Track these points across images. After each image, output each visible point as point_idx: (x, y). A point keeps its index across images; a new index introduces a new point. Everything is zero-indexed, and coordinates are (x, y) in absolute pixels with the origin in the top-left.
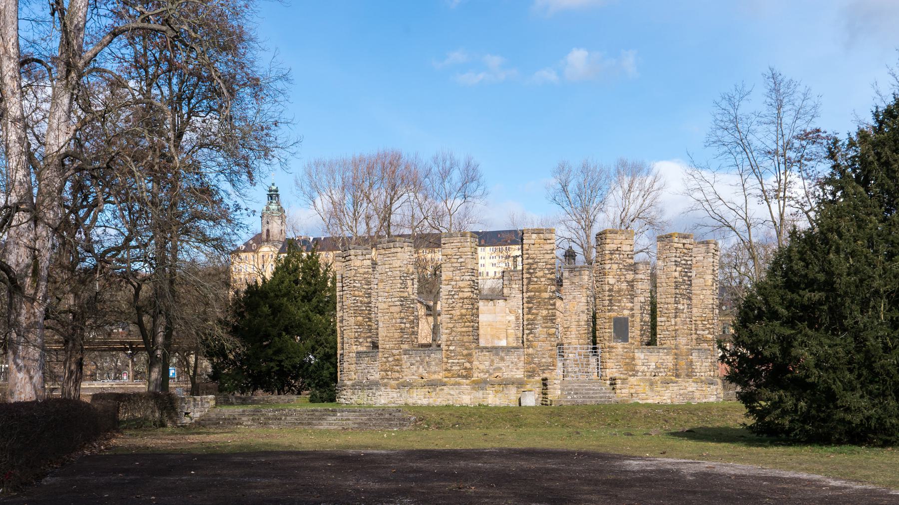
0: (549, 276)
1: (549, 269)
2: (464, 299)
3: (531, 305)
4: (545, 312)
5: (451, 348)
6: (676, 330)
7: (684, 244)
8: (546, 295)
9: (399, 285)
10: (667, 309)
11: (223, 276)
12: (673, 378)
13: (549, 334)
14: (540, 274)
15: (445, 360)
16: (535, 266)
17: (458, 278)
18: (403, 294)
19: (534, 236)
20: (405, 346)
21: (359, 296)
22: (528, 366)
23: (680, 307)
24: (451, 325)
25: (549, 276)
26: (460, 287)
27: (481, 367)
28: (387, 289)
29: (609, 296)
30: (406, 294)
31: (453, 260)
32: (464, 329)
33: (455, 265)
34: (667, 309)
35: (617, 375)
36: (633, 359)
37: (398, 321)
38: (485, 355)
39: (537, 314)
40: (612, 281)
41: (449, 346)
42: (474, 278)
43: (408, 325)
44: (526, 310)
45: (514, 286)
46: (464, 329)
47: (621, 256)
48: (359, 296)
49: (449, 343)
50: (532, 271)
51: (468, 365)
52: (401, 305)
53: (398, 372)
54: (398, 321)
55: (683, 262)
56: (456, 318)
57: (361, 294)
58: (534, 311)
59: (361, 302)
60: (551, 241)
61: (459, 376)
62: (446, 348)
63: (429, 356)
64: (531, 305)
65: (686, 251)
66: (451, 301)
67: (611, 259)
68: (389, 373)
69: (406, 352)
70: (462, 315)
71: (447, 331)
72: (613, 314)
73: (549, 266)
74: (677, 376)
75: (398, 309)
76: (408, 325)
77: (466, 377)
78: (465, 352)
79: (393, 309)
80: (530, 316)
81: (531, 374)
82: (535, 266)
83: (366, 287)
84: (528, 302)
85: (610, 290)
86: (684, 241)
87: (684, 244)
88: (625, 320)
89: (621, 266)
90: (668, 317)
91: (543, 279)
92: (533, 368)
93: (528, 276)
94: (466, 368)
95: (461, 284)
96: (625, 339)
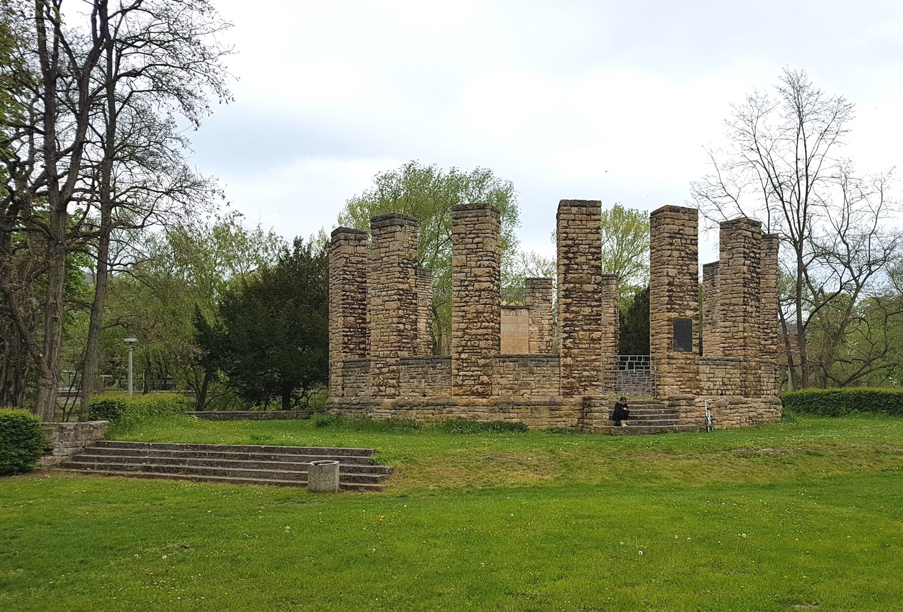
0: (593, 262)
1: (593, 254)
2: (480, 290)
3: (569, 301)
4: (587, 310)
5: (463, 356)
6: (745, 338)
7: (753, 232)
8: (589, 288)
9: (398, 275)
10: (733, 311)
11: (208, 284)
12: (742, 397)
13: (593, 340)
14: (582, 259)
15: (455, 372)
16: (575, 249)
17: (473, 264)
18: (401, 286)
19: (574, 210)
20: (405, 354)
21: (350, 291)
22: (565, 381)
23: (749, 309)
24: (463, 326)
25: (593, 262)
26: (475, 276)
27: (502, 381)
28: (383, 279)
29: (668, 291)
30: (406, 286)
31: (467, 240)
32: (481, 331)
33: (469, 246)
34: (733, 311)
35: (678, 394)
36: (697, 373)
37: (395, 320)
38: (508, 367)
39: (577, 312)
40: (673, 272)
41: (460, 353)
42: (494, 265)
43: (408, 327)
44: (563, 307)
45: (537, 295)
46: (481, 331)
47: (684, 241)
48: (350, 291)
49: (460, 349)
50: (571, 255)
51: (485, 379)
52: (399, 300)
53: (394, 387)
54: (395, 320)
55: (752, 255)
56: (469, 316)
57: (352, 288)
58: (574, 308)
59: (353, 298)
60: (596, 217)
61: (473, 393)
62: (457, 356)
63: (434, 367)
64: (569, 301)
65: (754, 242)
66: (464, 294)
67: (671, 244)
68: (383, 388)
69: (404, 361)
70: (477, 312)
71: (460, 334)
72: (674, 315)
73: (593, 250)
74: (746, 395)
75: (394, 305)
76: (408, 327)
77: (482, 395)
78: (482, 362)
79: (388, 305)
80: (568, 315)
81: (569, 391)
82: (575, 249)
83: (359, 279)
84: (565, 297)
85: (669, 284)
86: (753, 229)
87: (753, 232)
88: (688, 322)
89: (683, 254)
90: (734, 322)
91: (584, 267)
92: (572, 383)
93: (567, 262)
94: (482, 383)
95: (478, 271)
96: (688, 349)
